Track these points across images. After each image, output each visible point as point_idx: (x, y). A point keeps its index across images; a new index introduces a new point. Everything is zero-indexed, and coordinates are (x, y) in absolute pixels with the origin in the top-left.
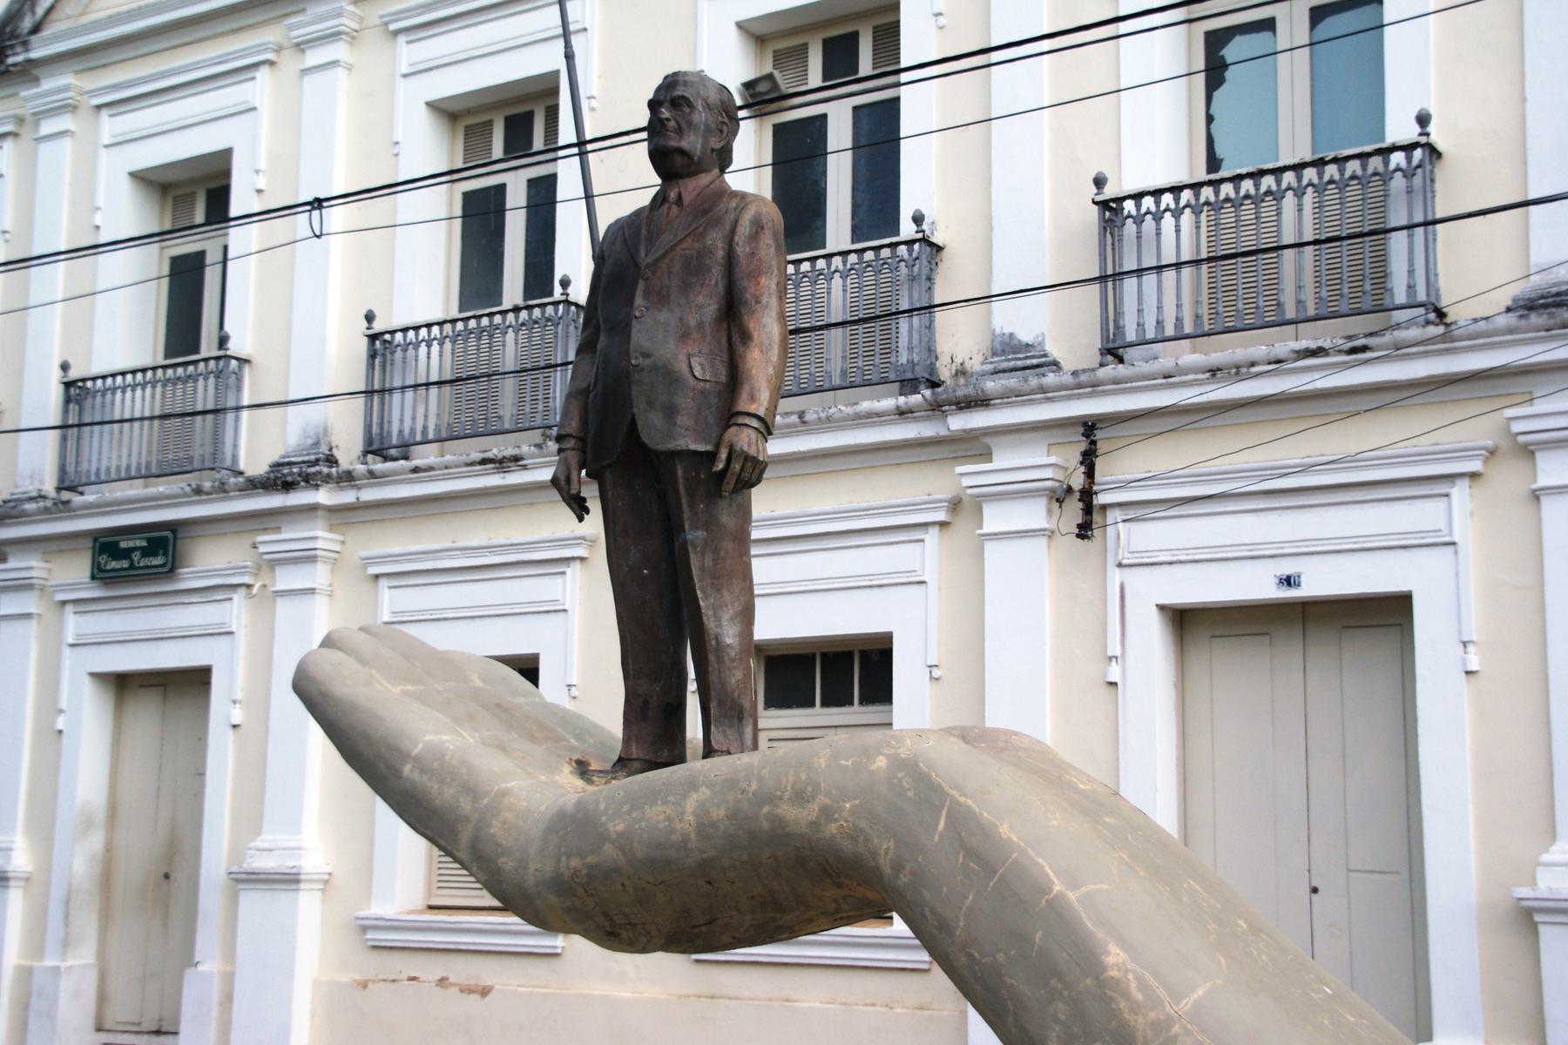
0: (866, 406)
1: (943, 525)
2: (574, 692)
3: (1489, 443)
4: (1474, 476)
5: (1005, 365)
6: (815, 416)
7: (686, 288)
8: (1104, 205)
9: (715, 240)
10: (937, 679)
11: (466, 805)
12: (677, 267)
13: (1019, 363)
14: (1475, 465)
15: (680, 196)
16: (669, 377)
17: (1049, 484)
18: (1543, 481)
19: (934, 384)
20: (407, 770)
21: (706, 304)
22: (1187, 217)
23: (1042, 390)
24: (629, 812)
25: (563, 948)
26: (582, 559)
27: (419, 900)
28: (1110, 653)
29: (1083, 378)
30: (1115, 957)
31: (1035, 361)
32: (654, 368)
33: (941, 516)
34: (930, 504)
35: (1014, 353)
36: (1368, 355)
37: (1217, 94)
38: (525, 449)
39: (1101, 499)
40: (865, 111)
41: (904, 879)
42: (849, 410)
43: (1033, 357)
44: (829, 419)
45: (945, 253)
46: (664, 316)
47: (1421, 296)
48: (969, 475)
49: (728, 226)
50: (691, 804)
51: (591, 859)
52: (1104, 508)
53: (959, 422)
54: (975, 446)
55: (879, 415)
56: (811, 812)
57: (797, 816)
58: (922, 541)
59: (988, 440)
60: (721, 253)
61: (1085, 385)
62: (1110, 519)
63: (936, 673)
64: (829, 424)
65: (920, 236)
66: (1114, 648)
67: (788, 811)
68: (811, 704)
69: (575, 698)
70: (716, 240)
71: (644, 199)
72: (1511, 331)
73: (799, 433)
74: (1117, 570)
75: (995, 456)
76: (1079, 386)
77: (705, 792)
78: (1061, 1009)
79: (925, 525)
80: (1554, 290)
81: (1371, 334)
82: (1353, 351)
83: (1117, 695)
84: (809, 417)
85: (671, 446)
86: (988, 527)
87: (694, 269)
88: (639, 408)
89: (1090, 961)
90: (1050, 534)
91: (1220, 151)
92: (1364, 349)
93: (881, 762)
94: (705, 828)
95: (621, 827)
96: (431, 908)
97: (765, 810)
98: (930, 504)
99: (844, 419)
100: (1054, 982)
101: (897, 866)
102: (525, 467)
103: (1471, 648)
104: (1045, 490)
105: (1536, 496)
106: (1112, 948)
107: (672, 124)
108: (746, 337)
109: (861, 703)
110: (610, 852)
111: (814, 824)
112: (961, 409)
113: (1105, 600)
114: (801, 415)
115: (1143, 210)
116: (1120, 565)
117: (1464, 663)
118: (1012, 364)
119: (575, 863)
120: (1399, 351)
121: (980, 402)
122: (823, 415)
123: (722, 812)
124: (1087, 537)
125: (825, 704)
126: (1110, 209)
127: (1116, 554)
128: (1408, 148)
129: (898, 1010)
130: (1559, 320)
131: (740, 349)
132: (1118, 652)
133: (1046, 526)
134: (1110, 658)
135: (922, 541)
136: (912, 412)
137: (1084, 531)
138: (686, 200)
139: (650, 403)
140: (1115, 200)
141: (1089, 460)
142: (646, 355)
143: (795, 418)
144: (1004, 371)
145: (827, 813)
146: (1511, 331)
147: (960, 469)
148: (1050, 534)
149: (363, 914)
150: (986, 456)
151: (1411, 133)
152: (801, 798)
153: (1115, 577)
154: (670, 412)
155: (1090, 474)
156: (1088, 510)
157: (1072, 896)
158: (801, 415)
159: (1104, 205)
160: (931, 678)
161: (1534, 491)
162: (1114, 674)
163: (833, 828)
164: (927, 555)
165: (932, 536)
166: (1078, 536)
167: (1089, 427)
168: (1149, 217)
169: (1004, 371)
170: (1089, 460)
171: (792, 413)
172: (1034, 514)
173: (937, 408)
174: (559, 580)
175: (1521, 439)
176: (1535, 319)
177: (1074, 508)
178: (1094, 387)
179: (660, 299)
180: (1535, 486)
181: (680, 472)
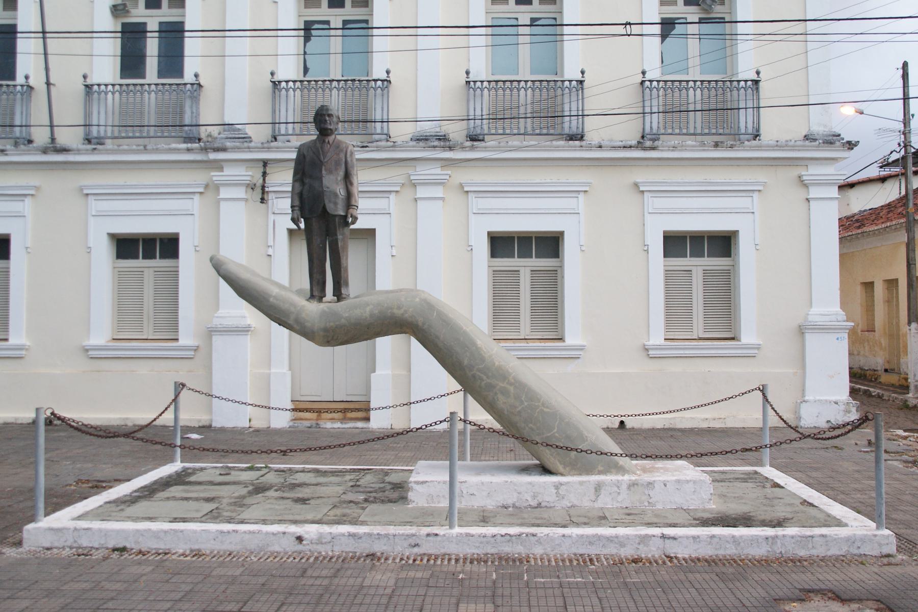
0: (174, 146)
1: (201, 193)
2: (29, 250)
3: (403, 182)
4: (397, 192)
5: (231, 136)
6: (151, 148)
7: (336, 169)
8: (86, 86)
9: (342, 156)
10: (198, 251)
11: (292, 309)
12: (333, 163)
13: (237, 136)
14: (398, 189)
15: (329, 141)
16: (336, 195)
17: (248, 182)
18: (418, 196)
19: (200, 140)
20: (271, 299)
21: (342, 173)
22: (117, 95)
23: (249, 148)
24: (349, 311)
25: (25, 355)
26: (32, 195)
27: (109, 337)
28: (269, 245)
29: (266, 145)
30: (479, 342)
31: (243, 136)
32: (330, 191)
33: (201, 190)
34: (198, 185)
35: (234, 131)
36: (367, 149)
37: (308, 44)
38: (8, 147)
39: (267, 189)
40: (164, 24)
41: (425, 327)
42: (166, 147)
43: (242, 134)
44: (157, 149)
45: (203, 89)
46: (332, 177)
47: (385, 132)
48: (216, 176)
49: (344, 151)
50: (368, 309)
51: (337, 323)
52: (268, 192)
53: (213, 156)
54: (218, 165)
55: (179, 150)
56: (401, 311)
57: (398, 312)
58: (193, 199)
59: (222, 163)
60: (344, 160)
61: (263, 148)
62: (270, 197)
63: (197, 249)
64: (157, 151)
65: (197, 82)
66: (271, 243)
67: (395, 311)
68: (155, 258)
69: (29, 253)
70: (342, 156)
71: (314, 137)
72: (413, 147)
73: (144, 153)
74: (273, 215)
75: (225, 169)
76: (264, 148)
77: (371, 307)
78: (468, 354)
79: (194, 193)
80: (425, 134)
81: (369, 142)
82: (363, 147)
83: (271, 260)
84: (149, 147)
85: (336, 213)
86: (222, 196)
87: (337, 163)
88: (326, 202)
89: (474, 344)
90: (246, 200)
91: (308, 65)
92: (366, 147)
93: (417, 300)
94: (371, 315)
95: (347, 315)
96: (114, 339)
97: (390, 311)
98: (198, 185)
99: (163, 150)
100: (466, 349)
101: (424, 324)
102: (6, 155)
103: (393, 248)
104: (246, 184)
105: (416, 200)
106: (478, 340)
107: (328, 122)
108: (352, 184)
109: (690, 257)
110: (343, 321)
111: (403, 314)
112: (214, 151)
113: (267, 225)
114: (145, 146)
115: (289, 87)
116: (274, 213)
117: (391, 253)
118: (233, 136)
119: (332, 324)
120: (379, 149)
121: (224, 149)
122: (154, 147)
123: (377, 312)
124: (264, 203)
125: (144, 258)
126: (276, 84)
127: (272, 209)
128: (383, 81)
129: (181, 373)
130: (428, 145)
131: (349, 186)
132: (272, 244)
133: (245, 197)
134: (269, 246)
135: (193, 199)
136: (193, 150)
137: (263, 200)
138: (331, 142)
139: (330, 201)
140: (278, 82)
141: (264, 174)
142: (328, 188)
143: (142, 147)
144: (231, 138)
145: (406, 311)
146: (413, 147)
147: (213, 174)
148: (246, 200)
149: (84, 344)
150: (221, 169)
151: (384, 76)
152: (399, 308)
153: (272, 217)
154: (336, 204)
155: (264, 180)
156: (263, 192)
157: (468, 330)
158: (145, 146)
159: (86, 86)
160: (196, 251)
161: (415, 199)
162: (270, 252)
163: (407, 315)
164: (195, 204)
165: (197, 197)
166: (261, 202)
167: (265, 163)
168: (117, 93)
169: (231, 138)
170: (264, 174)
171: (141, 145)
172: (241, 193)
173: (205, 150)
174: (21, 204)
175: (413, 181)
176: (421, 144)
177: (258, 191)
178: (269, 149)
179: (330, 172)
180: (416, 197)
181: (337, 220)
